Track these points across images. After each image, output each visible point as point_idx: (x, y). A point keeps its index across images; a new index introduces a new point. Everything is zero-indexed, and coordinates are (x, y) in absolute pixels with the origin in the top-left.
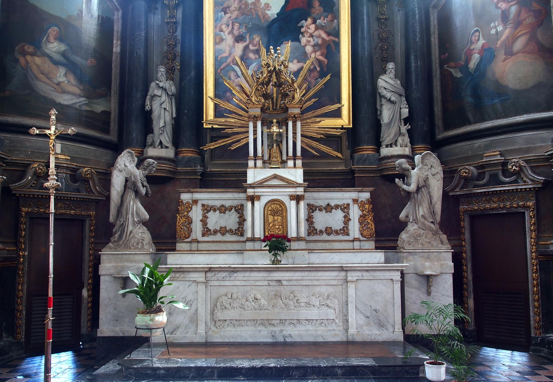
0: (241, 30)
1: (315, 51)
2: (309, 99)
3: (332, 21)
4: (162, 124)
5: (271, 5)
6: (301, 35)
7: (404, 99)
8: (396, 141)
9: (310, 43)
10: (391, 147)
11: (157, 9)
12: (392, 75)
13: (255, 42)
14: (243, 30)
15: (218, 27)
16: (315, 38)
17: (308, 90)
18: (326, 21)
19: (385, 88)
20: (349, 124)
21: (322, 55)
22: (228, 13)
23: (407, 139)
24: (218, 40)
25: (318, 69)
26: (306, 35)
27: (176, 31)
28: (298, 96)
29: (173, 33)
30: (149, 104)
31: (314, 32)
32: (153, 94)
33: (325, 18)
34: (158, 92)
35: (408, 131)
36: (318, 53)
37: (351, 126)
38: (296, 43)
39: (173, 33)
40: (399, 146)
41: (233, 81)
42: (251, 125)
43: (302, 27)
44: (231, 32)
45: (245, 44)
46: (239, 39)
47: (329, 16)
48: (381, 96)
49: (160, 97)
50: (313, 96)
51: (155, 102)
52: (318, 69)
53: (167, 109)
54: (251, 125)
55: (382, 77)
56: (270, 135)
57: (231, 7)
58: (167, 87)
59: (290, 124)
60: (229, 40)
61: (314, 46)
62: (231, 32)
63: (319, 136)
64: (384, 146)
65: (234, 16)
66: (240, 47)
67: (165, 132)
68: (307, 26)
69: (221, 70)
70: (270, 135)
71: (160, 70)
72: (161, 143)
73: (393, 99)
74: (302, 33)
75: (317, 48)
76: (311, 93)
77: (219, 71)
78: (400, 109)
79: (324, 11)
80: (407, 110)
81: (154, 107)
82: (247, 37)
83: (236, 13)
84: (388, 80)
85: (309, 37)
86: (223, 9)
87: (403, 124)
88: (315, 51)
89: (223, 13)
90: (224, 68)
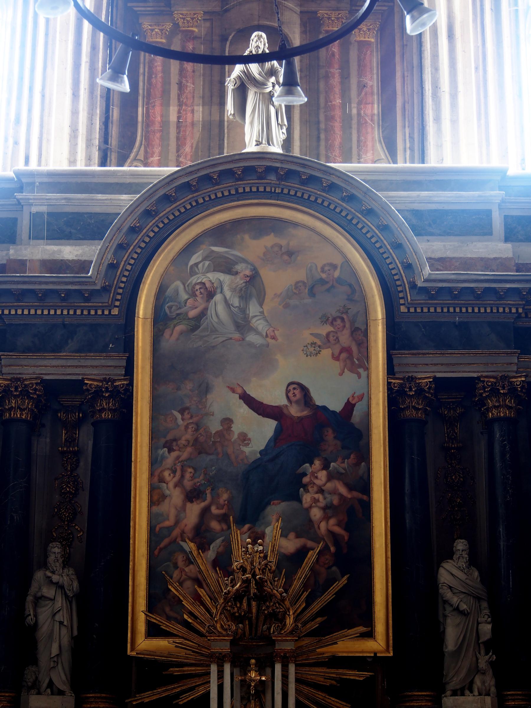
0: (196, 480)
1: (326, 518)
2: (313, 618)
3: (357, 464)
4: (55, 651)
5: (250, 436)
6: (302, 489)
7: (485, 604)
8: (472, 683)
9: (318, 504)
10: (463, 694)
11: (43, 426)
12: (462, 563)
13: (221, 501)
14: (200, 479)
15: (157, 473)
16: (327, 495)
17: (309, 601)
18: (345, 465)
19: (450, 587)
20: (387, 650)
21: (339, 524)
22: (174, 450)
23: (490, 681)
24: (156, 497)
25: (332, 549)
26: (310, 489)
27: (77, 466)
28: (290, 621)
29: (72, 471)
30: (32, 613)
31: (325, 485)
32: (39, 594)
33: (344, 459)
34: (49, 592)
35: (491, 664)
36: (332, 521)
37: (391, 654)
38: (294, 504)
39: (72, 471)
40: (476, 693)
41: (182, 570)
42: (214, 668)
43: (304, 474)
44: (179, 484)
45: (203, 505)
46: (193, 495)
47: (352, 456)
48: (446, 602)
49: (51, 599)
50: (319, 614)
51: (43, 609)
52: (332, 549)
53: (65, 623)
54: (214, 668)
55: (445, 565)
56: (245, 684)
57: (180, 439)
58: (66, 584)
59: (278, 667)
60: (176, 497)
61: (325, 509)
62: (179, 484)
63: (328, 683)
64: (449, 693)
65: (185, 455)
66: (193, 511)
67: (60, 666)
68: (313, 473)
69: (161, 550)
70: (245, 684)
71: (53, 550)
72: (51, 684)
73: (464, 607)
74: (305, 486)
75: (330, 512)
76: (316, 606)
77: (156, 552)
78: (478, 623)
79: (343, 447)
80: (489, 627)
81: (42, 618)
82: (208, 492)
83: (189, 449)
84: (455, 571)
85: (317, 493)
86: (166, 442)
87: (483, 652)
88: (326, 518)
89: (166, 449)
90: (166, 547)
